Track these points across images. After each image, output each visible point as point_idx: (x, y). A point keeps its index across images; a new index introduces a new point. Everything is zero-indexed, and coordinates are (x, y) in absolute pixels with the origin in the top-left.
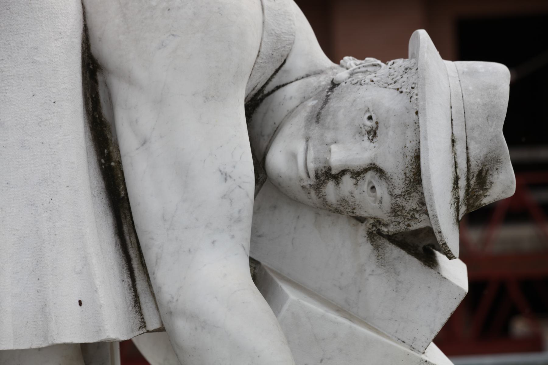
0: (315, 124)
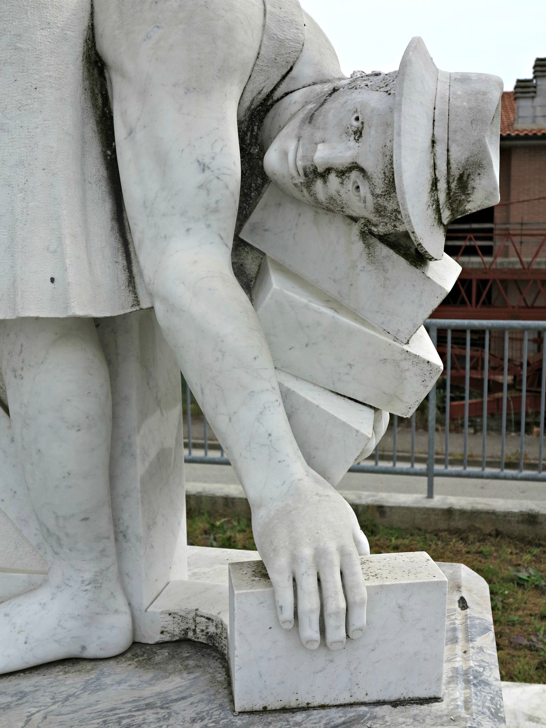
0: (307, 125)
